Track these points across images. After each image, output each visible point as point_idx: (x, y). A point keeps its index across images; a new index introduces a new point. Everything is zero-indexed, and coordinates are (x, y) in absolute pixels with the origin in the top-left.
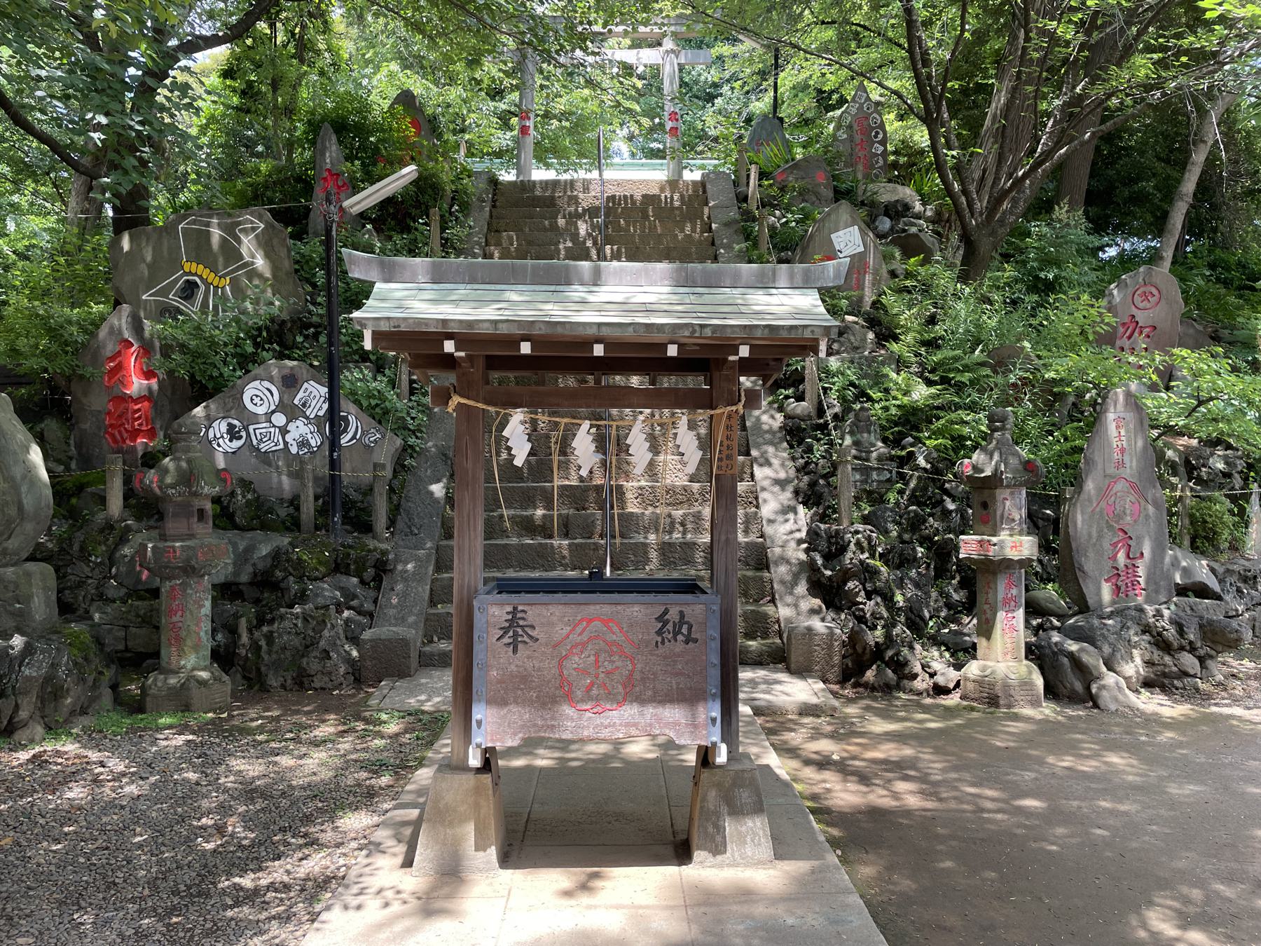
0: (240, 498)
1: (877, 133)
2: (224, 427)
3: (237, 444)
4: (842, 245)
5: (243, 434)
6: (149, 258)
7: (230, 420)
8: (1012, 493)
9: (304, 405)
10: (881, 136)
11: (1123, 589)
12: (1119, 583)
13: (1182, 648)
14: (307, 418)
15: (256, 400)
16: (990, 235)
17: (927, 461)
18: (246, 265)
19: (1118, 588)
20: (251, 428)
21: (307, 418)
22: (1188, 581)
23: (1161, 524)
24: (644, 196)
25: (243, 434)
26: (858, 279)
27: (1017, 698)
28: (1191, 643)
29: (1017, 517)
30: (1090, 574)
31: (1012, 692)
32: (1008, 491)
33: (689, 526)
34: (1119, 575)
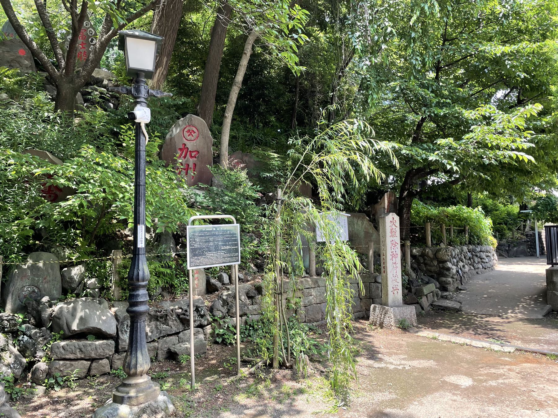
16: (70, 82)
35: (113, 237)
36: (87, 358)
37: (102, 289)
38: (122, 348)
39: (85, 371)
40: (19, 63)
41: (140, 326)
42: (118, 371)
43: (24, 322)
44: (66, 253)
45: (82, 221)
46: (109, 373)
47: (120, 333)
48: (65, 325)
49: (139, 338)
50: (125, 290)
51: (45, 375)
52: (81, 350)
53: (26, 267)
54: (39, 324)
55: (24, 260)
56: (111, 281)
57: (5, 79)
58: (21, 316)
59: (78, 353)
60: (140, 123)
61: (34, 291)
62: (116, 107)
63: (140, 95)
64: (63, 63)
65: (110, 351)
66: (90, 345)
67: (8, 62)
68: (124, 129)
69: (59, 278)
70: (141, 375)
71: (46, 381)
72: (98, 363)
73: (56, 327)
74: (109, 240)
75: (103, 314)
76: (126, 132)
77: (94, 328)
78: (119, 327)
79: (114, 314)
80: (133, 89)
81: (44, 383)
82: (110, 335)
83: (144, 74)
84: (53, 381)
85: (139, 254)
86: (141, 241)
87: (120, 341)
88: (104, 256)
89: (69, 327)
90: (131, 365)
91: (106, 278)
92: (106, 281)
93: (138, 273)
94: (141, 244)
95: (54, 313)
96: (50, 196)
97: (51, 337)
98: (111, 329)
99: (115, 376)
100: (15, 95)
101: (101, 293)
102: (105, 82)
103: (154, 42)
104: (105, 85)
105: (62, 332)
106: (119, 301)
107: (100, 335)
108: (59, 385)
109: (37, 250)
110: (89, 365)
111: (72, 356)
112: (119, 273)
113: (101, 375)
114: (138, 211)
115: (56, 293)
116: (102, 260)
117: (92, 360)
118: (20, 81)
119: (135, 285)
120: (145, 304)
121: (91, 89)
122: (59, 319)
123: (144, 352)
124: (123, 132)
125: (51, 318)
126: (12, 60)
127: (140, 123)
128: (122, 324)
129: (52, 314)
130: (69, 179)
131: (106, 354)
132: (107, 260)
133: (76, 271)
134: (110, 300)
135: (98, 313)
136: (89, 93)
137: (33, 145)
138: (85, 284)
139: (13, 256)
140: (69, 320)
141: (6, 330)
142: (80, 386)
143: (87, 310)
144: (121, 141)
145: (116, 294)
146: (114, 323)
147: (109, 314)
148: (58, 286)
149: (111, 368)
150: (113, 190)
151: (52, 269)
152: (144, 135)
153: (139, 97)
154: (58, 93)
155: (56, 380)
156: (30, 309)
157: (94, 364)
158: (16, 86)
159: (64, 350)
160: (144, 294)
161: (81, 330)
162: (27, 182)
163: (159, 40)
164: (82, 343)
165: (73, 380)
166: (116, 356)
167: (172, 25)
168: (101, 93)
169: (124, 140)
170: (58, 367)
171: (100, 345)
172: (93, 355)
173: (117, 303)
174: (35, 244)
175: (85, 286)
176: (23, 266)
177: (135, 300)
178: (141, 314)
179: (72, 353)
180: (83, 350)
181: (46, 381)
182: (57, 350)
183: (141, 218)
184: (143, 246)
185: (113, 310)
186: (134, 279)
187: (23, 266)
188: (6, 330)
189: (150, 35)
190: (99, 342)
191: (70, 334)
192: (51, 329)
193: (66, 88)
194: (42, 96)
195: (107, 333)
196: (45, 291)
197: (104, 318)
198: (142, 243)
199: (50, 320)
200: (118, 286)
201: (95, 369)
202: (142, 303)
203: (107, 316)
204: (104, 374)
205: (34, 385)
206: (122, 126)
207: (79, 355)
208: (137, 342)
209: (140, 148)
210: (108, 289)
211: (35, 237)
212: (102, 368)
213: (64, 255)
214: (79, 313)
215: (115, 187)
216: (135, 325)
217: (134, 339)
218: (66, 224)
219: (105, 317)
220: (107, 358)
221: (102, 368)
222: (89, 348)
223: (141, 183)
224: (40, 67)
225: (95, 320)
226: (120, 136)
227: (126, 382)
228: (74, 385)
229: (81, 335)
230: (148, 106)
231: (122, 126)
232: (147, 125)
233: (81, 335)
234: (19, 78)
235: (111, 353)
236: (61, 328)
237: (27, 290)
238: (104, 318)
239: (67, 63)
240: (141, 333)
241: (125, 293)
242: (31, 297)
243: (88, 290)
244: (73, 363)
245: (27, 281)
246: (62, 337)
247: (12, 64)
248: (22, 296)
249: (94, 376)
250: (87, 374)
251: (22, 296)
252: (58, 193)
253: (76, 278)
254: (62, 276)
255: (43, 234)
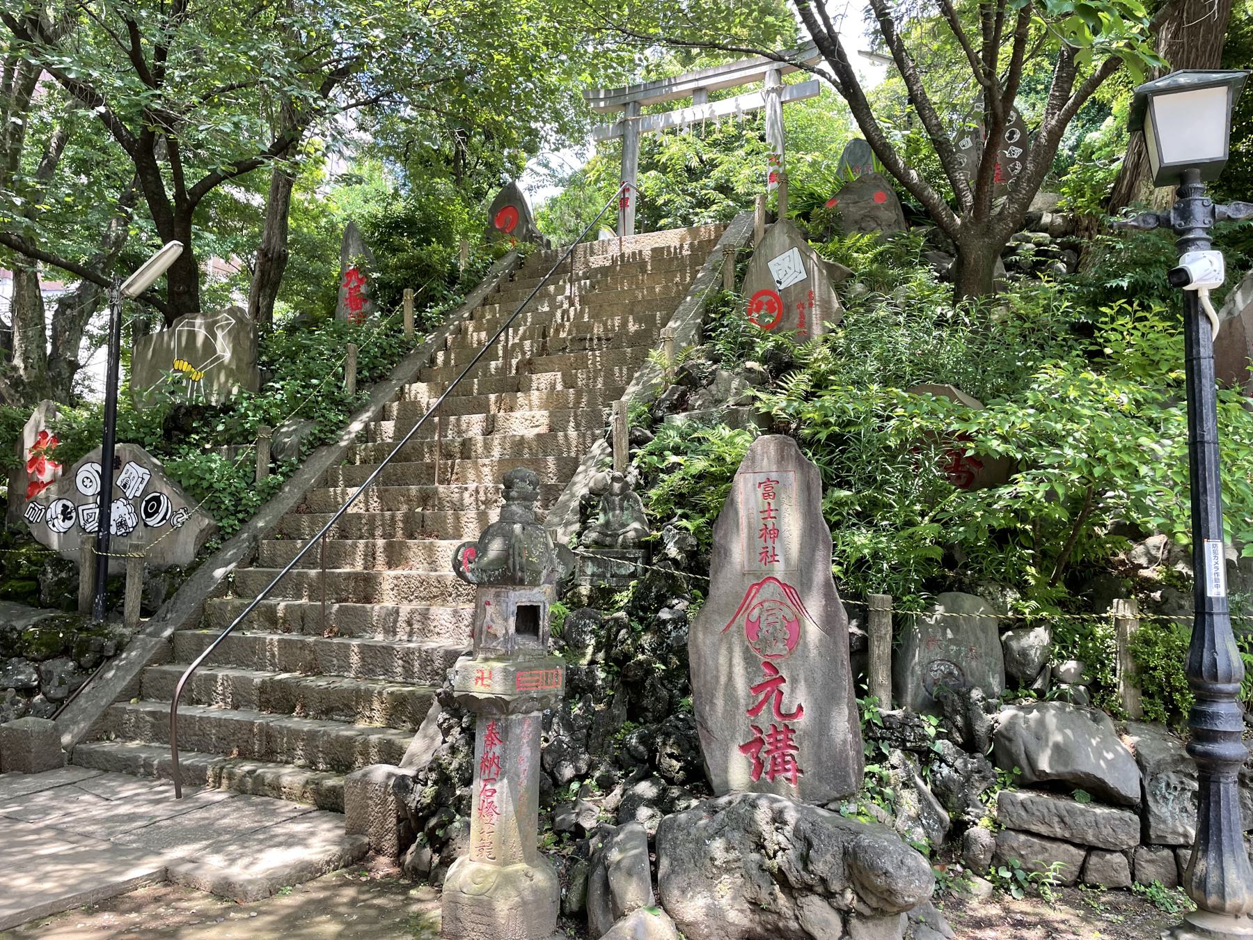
0: (50, 576)
1: (1013, 133)
2: (60, 509)
3: (69, 523)
4: (782, 273)
5: (74, 514)
6: (49, 351)
7: (65, 502)
8: (497, 595)
9: (125, 486)
10: (1017, 137)
11: (768, 767)
12: (763, 755)
13: (809, 889)
14: (126, 499)
15: (87, 482)
16: (984, 235)
17: (681, 550)
18: (218, 358)
19: (760, 764)
20: (80, 509)
21: (126, 499)
22: (1061, 769)
23: (834, 661)
24: (653, 250)
25: (74, 514)
26: (802, 316)
27: (468, 925)
28: (823, 881)
29: (500, 632)
30: (717, 734)
31: (462, 915)
32: (493, 590)
33: (416, 626)
34: (761, 741)
35: (1104, 568)
36: (1077, 841)
37: (1094, 686)
38: (1158, 836)
39: (1075, 870)
40: (875, 219)
41: (1227, 792)
42: (1154, 890)
43: (939, 736)
44: (1009, 600)
45: (1033, 530)
46: (1129, 890)
47: (1149, 799)
48: (1023, 756)
49: (1224, 821)
50: (1151, 696)
51: (989, 856)
52: (1062, 821)
53: (933, 622)
54: (970, 745)
55: (929, 607)
56: (1114, 670)
57: (855, 255)
58: (934, 721)
59: (1056, 825)
60: (1196, 292)
61: (951, 673)
62: (1073, 268)
63: (1193, 224)
64: (969, 199)
65: (1131, 838)
66: (1082, 813)
67: (856, 222)
68: (1105, 315)
69: (999, 651)
70: (1237, 917)
71: (992, 870)
72: (1102, 857)
73: (1002, 755)
74: (1095, 574)
75: (1105, 745)
76: (1113, 320)
77: (1088, 775)
78: (1146, 783)
79: (1131, 751)
80: (1172, 214)
81: (989, 873)
82: (1126, 798)
83: (1198, 171)
84: (1008, 875)
85: (1211, 615)
86: (1217, 580)
87: (1151, 819)
88: (1086, 611)
89: (1032, 763)
90: (1209, 886)
91: (1103, 664)
92: (1102, 670)
93: (1215, 660)
94: (1216, 588)
95: (998, 727)
96: (959, 477)
97: (994, 776)
98: (1128, 783)
99: (1146, 900)
100: (877, 282)
101: (1092, 697)
102: (1047, 219)
103: (1225, 89)
104: (1045, 224)
105: (1016, 771)
106: (1138, 720)
107: (1102, 794)
108: (1020, 887)
109: (950, 589)
110: (1082, 859)
111: (1043, 830)
112: (1135, 655)
113: (1110, 889)
114: (1202, 507)
115: (996, 683)
116: (1084, 620)
117: (1090, 849)
118: (881, 254)
119: (1209, 690)
120: (1236, 741)
121: (1017, 240)
122: (1010, 740)
123: (1240, 860)
124: (1106, 323)
125: (995, 736)
126: (864, 217)
127: (1196, 292)
128: (1155, 778)
129: (992, 728)
130: (1005, 439)
131: (1122, 843)
132: (1100, 620)
133: (1038, 638)
134: (1115, 715)
135: (1094, 742)
136: (1013, 251)
137: (923, 375)
138: (1054, 673)
139: (908, 597)
140: (1032, 747)
141: (908, 744)
142: (1064, 901)
143: (1068, 732)
144: (1100, 344)
145: (1130, 703)
146: (1136, 773)
147: (1119, 749)
148: (998, 668)
149: (1133, 880)
150: (1126, 458)
151: (983, 631)
152: (1208, 318)
153: (1190, 230)
154: (960, 264)
155: (1014, 875)
156: (950, 709)
157: (1094, 860)
158: (875, 266)
159: (1026, 811)
160: (1233, 715)
161: (1058, 775)
162: (917, 449)
163: (1236, 80)
164: (1063, 803)
165: (1051, 884)
166: (1143, 851)
167: (1206, 41)
168: (1038, 244)
169: (1107, 340)
170: (1015, 845)
171: (1108, 819)
172: (1091, 838)
173: (1134, 725)
174: (944, 577)
175: (1055, 679)
176: (928, 620)
177: (1209, 727)
178: (1227, 762)
179: (1043, 822)
180: (1067, 819)
181: (992, 870)
182: (1010, 808)
183: (1213, 525)
184: (1223, 594)
185: (1129, 741)
186: (1205, 674)
187: (928, 620)
188: (908, 744)
189: (1214, 75)
190: (1101, 811)
191: (1035, 779)
192: (993, 759)
193: (976, 249)
194: (922, 276)
195: (1118, 793)
196: (972, 675)
197: (1110, 756)
198: (1217, 586)
199: (991, 740)
200: (1134, 686)
201: (1097, 871)
202: (1227, 735)
203: (1115, 752)
204: (1117, 889)
205: (969, 872)
206: (1103, 309)
207: (1059, 831)
208: (1220, 830)
209: (1199, 352)
210: (1111, 688)
211: (949, 561)
212: (1113, 873)
213: (1004, 602)
214: (1048, 731)
215: (1126, 449)
216: (1213, 787)
217: (1212, 821)
218: (1002, 538)
219: (1112, 754)
220: (1123, 851)
221: (1113, 873)
222: (1081, 820)
223: (1207, 438)
224: (913, 218)
225: (1088, 756)
226: (1097, 334)
227: (1197, 923)
228: (1051, 896)
229: (1059, 786)
230: (1214, 245)
231: (1103, 309)
232: (1213, 293)
233: (1059, 786)
234: (880, 249)
235: (1132, 843)
236: (1015, 762)
237: (939, 670)
238: (1110, 756)
239: (977, 198)
240: (1229, 811)
241: (1151, 704)
242: (946, 684)
243: (1064, 686)
244: (1048, 845)
245: (938, 650)
246: (1018, 781)
247: (863, 225)
248: (929, 681)
249: (1094, 887)
250: (1079, 877)
251: (929, 681)
252: (975, 470)
253: (1035, 656)
254: (1005, 646)
255: (957, 556)
